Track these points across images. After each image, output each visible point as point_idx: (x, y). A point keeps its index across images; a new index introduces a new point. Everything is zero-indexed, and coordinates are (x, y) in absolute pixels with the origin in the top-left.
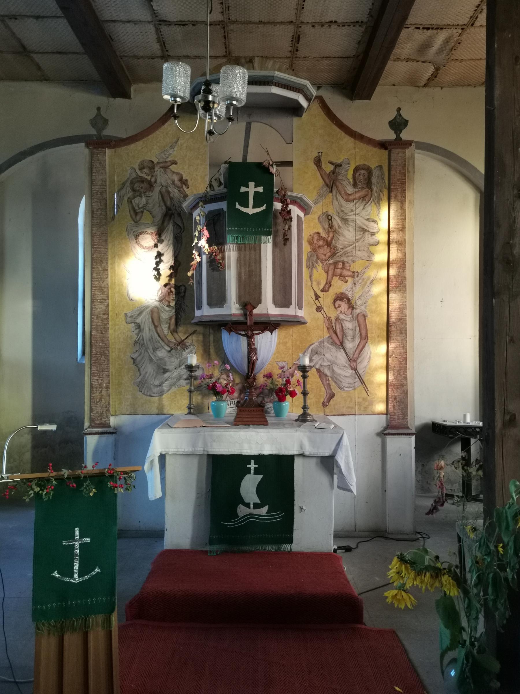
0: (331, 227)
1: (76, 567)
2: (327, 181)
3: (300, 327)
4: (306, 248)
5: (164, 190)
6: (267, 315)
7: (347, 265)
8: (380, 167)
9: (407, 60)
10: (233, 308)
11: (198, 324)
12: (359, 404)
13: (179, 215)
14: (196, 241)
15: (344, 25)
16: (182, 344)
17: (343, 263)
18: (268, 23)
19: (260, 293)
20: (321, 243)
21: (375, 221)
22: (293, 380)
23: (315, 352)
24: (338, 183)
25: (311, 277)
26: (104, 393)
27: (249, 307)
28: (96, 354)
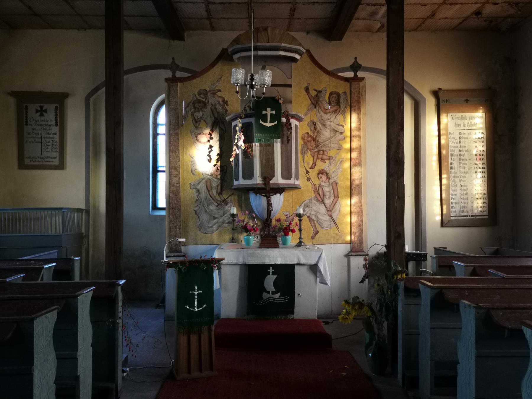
0: (315, 129)
1: (196, 304)
2: (313, 101)
3: (297, 190)
4: (300, 142)
5: (213, 107)
6: (278, 184)
7: (326, 152)
8: (345, 93)
9: (364, 19)
10: (258, 180)
11: (234, 189)
12: (334, 237)
13: (223, 122)
14: (236, 141)
15: (322, 3)
16: (225, 202)
17: (323, 151)
18: (276, 3)
19: (274, 171)
20: (310, 139)
21: (342, 126)
22: (293, 223)
23: (307, 206)
24: (319, 103)
25: (303, 159)
26: (178, 232)
27: (267, 179)
28: (173, 208)
